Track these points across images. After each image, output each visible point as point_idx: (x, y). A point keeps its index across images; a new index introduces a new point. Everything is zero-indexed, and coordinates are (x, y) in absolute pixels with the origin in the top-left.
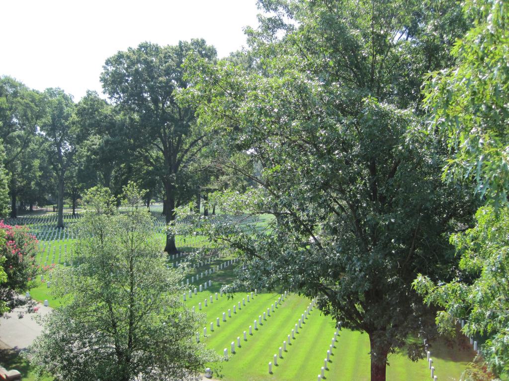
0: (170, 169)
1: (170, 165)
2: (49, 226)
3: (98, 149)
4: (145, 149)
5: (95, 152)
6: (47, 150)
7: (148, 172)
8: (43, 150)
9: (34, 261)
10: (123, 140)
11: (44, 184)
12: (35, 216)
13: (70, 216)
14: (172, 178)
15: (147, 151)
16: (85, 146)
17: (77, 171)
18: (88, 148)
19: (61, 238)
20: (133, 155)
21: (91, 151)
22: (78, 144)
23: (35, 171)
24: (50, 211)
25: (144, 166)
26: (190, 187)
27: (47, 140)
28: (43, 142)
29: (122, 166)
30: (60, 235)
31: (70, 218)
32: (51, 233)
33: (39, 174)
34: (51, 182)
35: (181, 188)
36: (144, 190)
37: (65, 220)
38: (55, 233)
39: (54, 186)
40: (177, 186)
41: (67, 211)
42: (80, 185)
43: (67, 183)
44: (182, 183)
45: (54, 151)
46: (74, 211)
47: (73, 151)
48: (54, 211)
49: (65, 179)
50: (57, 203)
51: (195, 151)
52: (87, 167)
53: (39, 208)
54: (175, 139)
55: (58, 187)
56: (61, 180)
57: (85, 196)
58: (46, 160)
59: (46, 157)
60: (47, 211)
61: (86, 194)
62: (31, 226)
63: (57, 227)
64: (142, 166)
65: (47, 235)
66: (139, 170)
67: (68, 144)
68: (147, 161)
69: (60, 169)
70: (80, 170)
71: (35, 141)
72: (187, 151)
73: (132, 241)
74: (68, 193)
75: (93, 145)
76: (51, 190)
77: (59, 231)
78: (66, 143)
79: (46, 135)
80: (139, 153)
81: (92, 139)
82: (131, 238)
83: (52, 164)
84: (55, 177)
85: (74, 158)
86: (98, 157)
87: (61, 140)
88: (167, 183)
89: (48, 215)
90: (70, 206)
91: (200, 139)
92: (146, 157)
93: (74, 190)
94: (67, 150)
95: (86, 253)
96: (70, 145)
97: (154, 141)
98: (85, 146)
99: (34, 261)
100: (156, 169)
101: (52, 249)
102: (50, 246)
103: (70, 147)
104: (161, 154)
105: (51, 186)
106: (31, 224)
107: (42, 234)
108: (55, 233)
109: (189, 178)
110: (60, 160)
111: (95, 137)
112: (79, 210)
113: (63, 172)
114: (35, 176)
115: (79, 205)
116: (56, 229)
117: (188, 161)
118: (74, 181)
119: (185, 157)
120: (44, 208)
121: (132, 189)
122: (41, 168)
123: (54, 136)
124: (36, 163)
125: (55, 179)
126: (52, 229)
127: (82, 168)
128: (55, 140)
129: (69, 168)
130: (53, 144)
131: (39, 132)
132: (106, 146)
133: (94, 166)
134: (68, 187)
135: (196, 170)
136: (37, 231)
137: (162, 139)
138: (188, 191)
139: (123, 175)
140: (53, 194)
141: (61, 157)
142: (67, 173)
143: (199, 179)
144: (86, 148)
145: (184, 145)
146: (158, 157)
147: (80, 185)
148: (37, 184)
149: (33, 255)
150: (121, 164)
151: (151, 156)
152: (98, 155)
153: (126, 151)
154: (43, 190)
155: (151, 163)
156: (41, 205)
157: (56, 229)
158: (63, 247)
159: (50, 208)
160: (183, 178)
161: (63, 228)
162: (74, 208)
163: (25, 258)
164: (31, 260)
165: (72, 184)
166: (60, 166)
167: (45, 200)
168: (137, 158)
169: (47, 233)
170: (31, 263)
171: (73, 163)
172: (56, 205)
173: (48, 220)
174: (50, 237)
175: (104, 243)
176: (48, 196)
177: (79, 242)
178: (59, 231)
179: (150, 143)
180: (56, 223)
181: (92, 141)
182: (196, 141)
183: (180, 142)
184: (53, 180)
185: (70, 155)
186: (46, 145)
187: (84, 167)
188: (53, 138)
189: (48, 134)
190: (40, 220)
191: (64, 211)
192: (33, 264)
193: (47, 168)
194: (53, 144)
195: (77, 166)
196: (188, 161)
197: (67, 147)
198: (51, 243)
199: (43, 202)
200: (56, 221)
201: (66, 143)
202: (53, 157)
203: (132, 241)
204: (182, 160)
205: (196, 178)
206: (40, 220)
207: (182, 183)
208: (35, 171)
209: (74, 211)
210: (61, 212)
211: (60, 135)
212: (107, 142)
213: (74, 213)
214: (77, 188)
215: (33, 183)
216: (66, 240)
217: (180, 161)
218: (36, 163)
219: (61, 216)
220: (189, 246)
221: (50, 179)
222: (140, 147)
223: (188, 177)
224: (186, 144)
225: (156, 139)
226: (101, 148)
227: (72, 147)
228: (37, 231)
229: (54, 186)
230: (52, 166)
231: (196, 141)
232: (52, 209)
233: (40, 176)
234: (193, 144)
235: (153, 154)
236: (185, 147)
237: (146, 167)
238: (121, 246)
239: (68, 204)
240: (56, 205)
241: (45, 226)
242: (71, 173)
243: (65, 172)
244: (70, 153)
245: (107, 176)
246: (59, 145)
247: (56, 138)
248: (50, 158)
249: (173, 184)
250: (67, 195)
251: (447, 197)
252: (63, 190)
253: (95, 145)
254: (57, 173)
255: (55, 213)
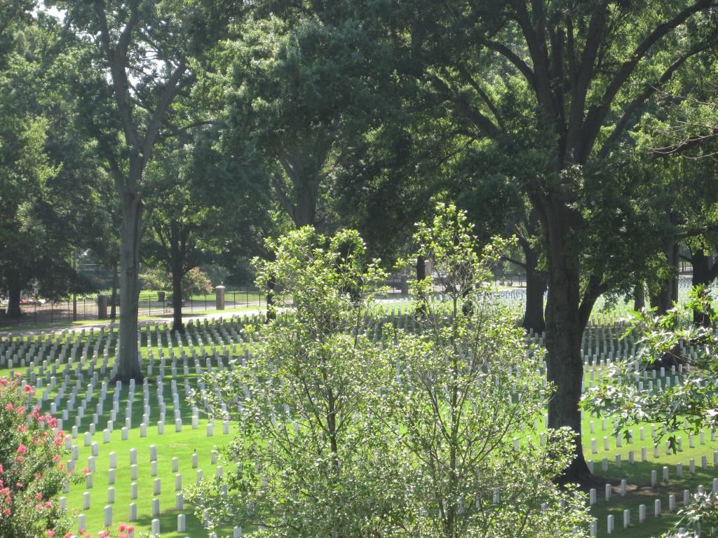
0: (563, 145)
1: (561, 128)
2: (86, 375)
3: (277, 71)
4: (459, 67)
5: (262, 85)
6: (73, 79)
7: (475, 162)
8: (60, 77)
9: (54, 514)
10: (373, 37)
11: (62, 212)
12: (30, 336)
13: (164, 335)
14: (566, 180)
15: (466, 77)
16: (228, 60)
17: (190, 159)
18: (236, 67)
19: (136, 422)
20: (411, 92)
21: (250, 82)
22: (197, 51)
23: (31, 163)
24: (86, 317)
25: (453, 134)
26: (644, 218)
27: (69, 38)
28: (57, 50)
29: (370, 136)
30: (129, 409)
31: (165, 344)
32: (94, 402)
33: (46, 172)
34: (92, 203)
35: (606, 223)
36: (497, 238)
37: (147, 352)
38: (109, 399)
39: (102, 220)
40: (587, 213)
41: (153, 316)
42: (202, 214)
43: (150, 208)
44: (608, 203)
45: (102, 82)
46: (178, 316)
47: (172, 79)
48: (102, 316)
49: (146, 192)
50: (114, 284)
51: (661, 69)
52: (235, 145)
53: (45, 305)
54: (581, 23)
55: (117, 221)
56: (132, 197)
57: (269, 265)
58: (72, 117)
59: (71, 110)
60: (75, 317)
61: (271, 257)
62: (21, 372)
63: (118, 377)
64: (446, 136)
65: (81, 409)
66: (437, 152)
67: (151, 54)
68: (467, 112)
69: (125, 153)
70: (204, 157)
71: (27, 45)
72: (630, 67)
73: (454, 443)
74: (152, 246)
75: (258, 55)
76: (90, 233)
77: (124, 395)
78: (143, 52)
79: (68, 20)
80: (437, 83)
81: (253, 34)
82: (449, 426)
83: (94, 132)
84: (107, 183)
85: (176, 106)
86: (277, 102)
87: (127, 39)
88: (551, 205)
89: (78, 330)
90: (161, 296)
91: (680, 19)
92: (465, 97)
93: (179, 232)
94: (148, 79)
95: (274, 483)
96: (160, 56)
97: (493, 34)
98: (228, 60)
99: (54, 514)
100: (509, 146)
101: (102, 464)
102: (95, 454)
103: (161, 64)
104: (520, 81)
105: (88, 221)
106: (17, 365)
107: (63, 404)
108: (109, 399)
109: (635, 181)
110: (123, 117)
111: (262, 23)
112: (197, 310)
113: (138, 166)
114: (33, 180)
115: (198, 292)
116: (112, 384)
117: (633, 111)
118: (179, 196)
119: (619, 97)
120: (65, 306)
121: (442, 227)
122: (54, 151)
123: (101, 24)
124: (36, 129)
125: (106, 189)
126: (98, 386)
127: (216, 147)
128: (105, 38)
129: (158, 147)
130: (97, 56)
131: (42, 8)
132: (308, 60)
133: (262, 140)
134: (158, 223)
135: (661, 155)
136: (39, 393)
137: (524, 24)
138: (633, 232)
139: (374, 171)
140: (99, 250)
141: (127, 104)
142: (152, 170)
143: (676, 184)
144: (230, 69)
145: (614, 47)
146: (510, 98)
147: (202, 214)
148: (42, 212)
149: (51, 491)
150: (366, 130)
151: (484, 96)
152: (276, 94)
153: (384, 78)
154: (61, 231)
155: (484, 123)
156: (53, 293)
157: (112, 384)
158: (144, 458)
159: (88, 304)
160: (612, 184)
161: (139, 382)
162: (177, 303)
163: (18, 501)
164: (42, 508)
165: (172, 210)
166: (122, 137)
167: (68, 271)
168: (430, 105)
169: (78, 401)
170: (42, 523)
171: (174, 128)
172: (108, 293)
173: (47, 352)
174: (93, 419)
175: (343, 448)
176: (80, 258)
177: (247, 445)
178: (124, 395)
179: (479, 40)
180: (112, 362)
181: (254, 42)
182: (664, 29)
183: (600, 33)
184: (95, 195)
185: (159, 96)
186: (69, 58)
187: (225, 144)
188: (93, 31)
189: (77, 18)
190: (52, 351)
191: (143, 315)
192: (50, 526)
193: (73, 148)
194: (97, 56)
195: (189, 139)
196: (633, 111)
197: (152, 65)
198: (97, 439)
199: (64, 282)
200: (111, 352)
201: (143, 52)
202: (98, 107)
203: (454, 443)
204: (606, 108)
205: (666, 182)
206: (52, 351)
207: (608, 203)
208: (31, 163)
209: (178, 316)
210: (130, 317)
211: (122, 14)
212: (310, 44)
213: (178, 324)
214: (191, 226)
215: (23, 208)
216: (152, 431)
217: (601, 113)
218: (36, 129)
219: (131, 333)
220: (638, 458)
221: (87, 193)
222: (441, 59)
223: (638, 178)
224: (623, 42)
225: (503, 25)
226: (288, 68)
227: (169, 65)
228: (39, 393)
229: (102, 220)
230: (95, 143)
231: (664, 29)
232: (93, 308)
233: (50, 182)
234: (649, 44)
235: (491, 88)
236: (621, 54)
237: (461, 141)
238: (413, 462)
239: (154, 288)
240: (108, 293)
241: (71, 374)
242: (167, 164)
243: (142, 163)
244: (159, 88)
245: (308, 177)
246: (118, 58)
247: (105, 30)
248: (86, 110)
249: (573, 206)
250: (154, 253)
251: (155, 71)
252: (137, 234)
253: (266, 55)
254: (114, 170)
255: (107, 323)
